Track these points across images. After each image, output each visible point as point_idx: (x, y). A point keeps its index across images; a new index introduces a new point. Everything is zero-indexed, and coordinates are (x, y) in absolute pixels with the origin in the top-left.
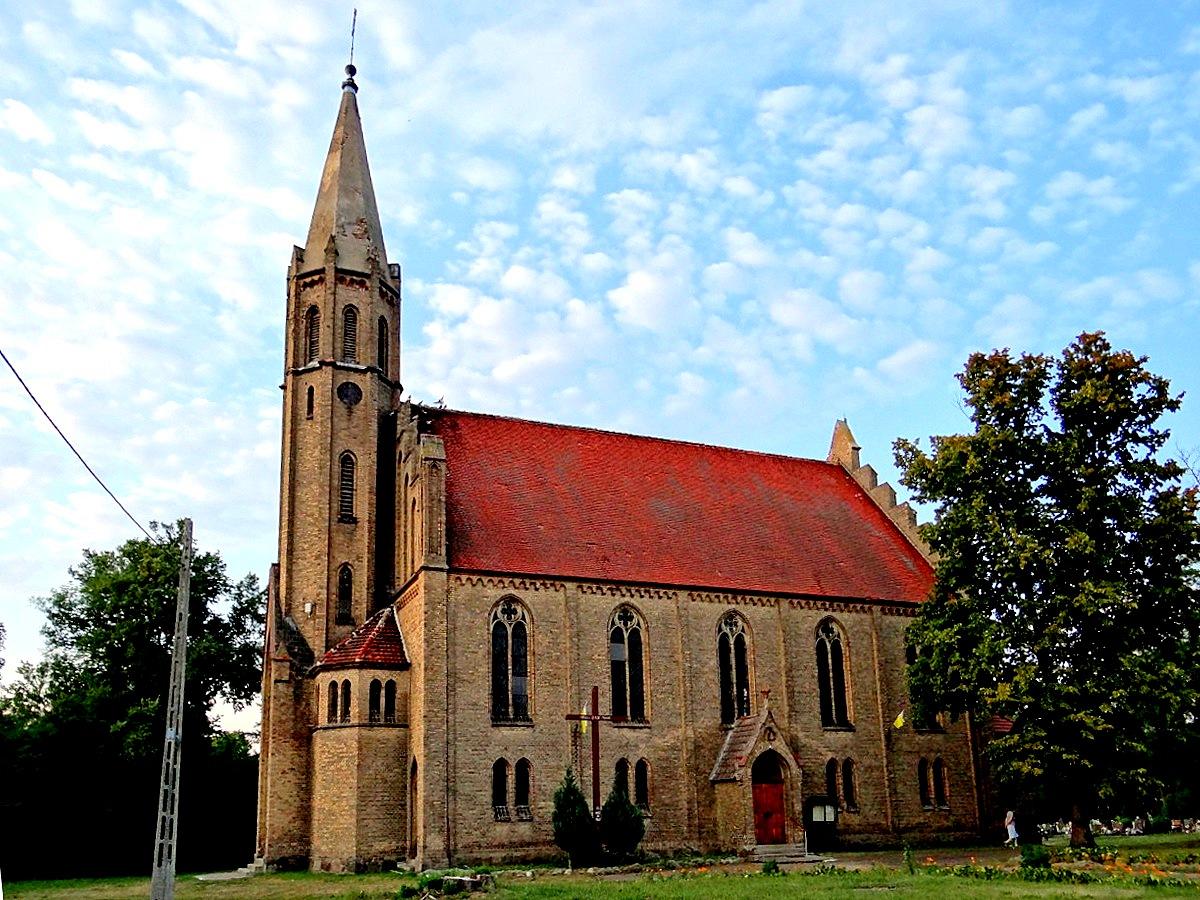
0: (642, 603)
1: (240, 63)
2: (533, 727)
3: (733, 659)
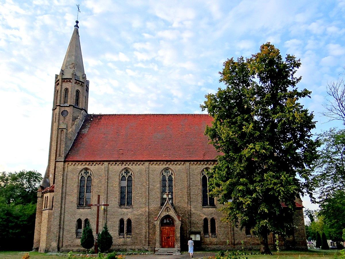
0: (132, 167)
1: (174, 29)
2: (91, 208)
3: (167, 184)
